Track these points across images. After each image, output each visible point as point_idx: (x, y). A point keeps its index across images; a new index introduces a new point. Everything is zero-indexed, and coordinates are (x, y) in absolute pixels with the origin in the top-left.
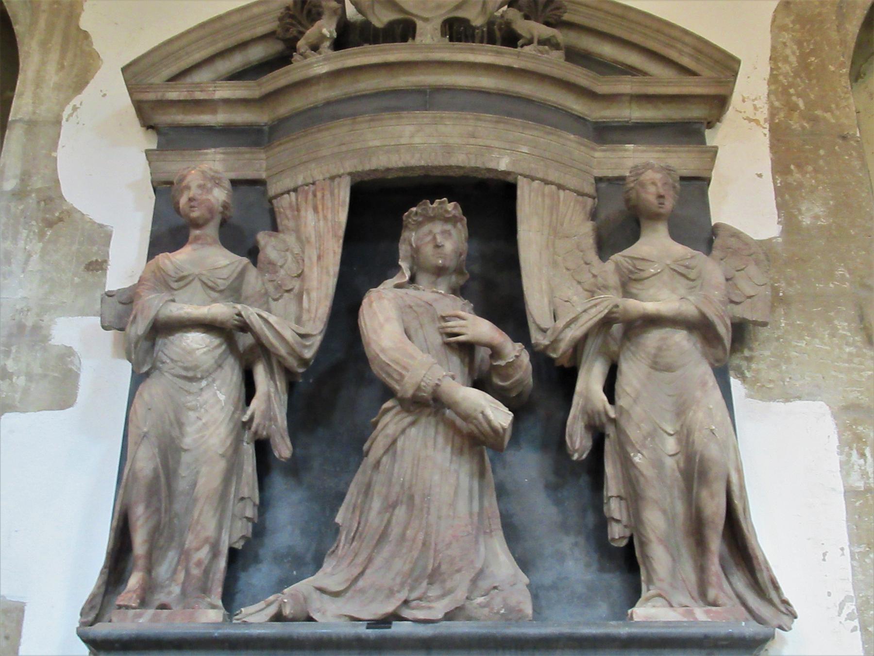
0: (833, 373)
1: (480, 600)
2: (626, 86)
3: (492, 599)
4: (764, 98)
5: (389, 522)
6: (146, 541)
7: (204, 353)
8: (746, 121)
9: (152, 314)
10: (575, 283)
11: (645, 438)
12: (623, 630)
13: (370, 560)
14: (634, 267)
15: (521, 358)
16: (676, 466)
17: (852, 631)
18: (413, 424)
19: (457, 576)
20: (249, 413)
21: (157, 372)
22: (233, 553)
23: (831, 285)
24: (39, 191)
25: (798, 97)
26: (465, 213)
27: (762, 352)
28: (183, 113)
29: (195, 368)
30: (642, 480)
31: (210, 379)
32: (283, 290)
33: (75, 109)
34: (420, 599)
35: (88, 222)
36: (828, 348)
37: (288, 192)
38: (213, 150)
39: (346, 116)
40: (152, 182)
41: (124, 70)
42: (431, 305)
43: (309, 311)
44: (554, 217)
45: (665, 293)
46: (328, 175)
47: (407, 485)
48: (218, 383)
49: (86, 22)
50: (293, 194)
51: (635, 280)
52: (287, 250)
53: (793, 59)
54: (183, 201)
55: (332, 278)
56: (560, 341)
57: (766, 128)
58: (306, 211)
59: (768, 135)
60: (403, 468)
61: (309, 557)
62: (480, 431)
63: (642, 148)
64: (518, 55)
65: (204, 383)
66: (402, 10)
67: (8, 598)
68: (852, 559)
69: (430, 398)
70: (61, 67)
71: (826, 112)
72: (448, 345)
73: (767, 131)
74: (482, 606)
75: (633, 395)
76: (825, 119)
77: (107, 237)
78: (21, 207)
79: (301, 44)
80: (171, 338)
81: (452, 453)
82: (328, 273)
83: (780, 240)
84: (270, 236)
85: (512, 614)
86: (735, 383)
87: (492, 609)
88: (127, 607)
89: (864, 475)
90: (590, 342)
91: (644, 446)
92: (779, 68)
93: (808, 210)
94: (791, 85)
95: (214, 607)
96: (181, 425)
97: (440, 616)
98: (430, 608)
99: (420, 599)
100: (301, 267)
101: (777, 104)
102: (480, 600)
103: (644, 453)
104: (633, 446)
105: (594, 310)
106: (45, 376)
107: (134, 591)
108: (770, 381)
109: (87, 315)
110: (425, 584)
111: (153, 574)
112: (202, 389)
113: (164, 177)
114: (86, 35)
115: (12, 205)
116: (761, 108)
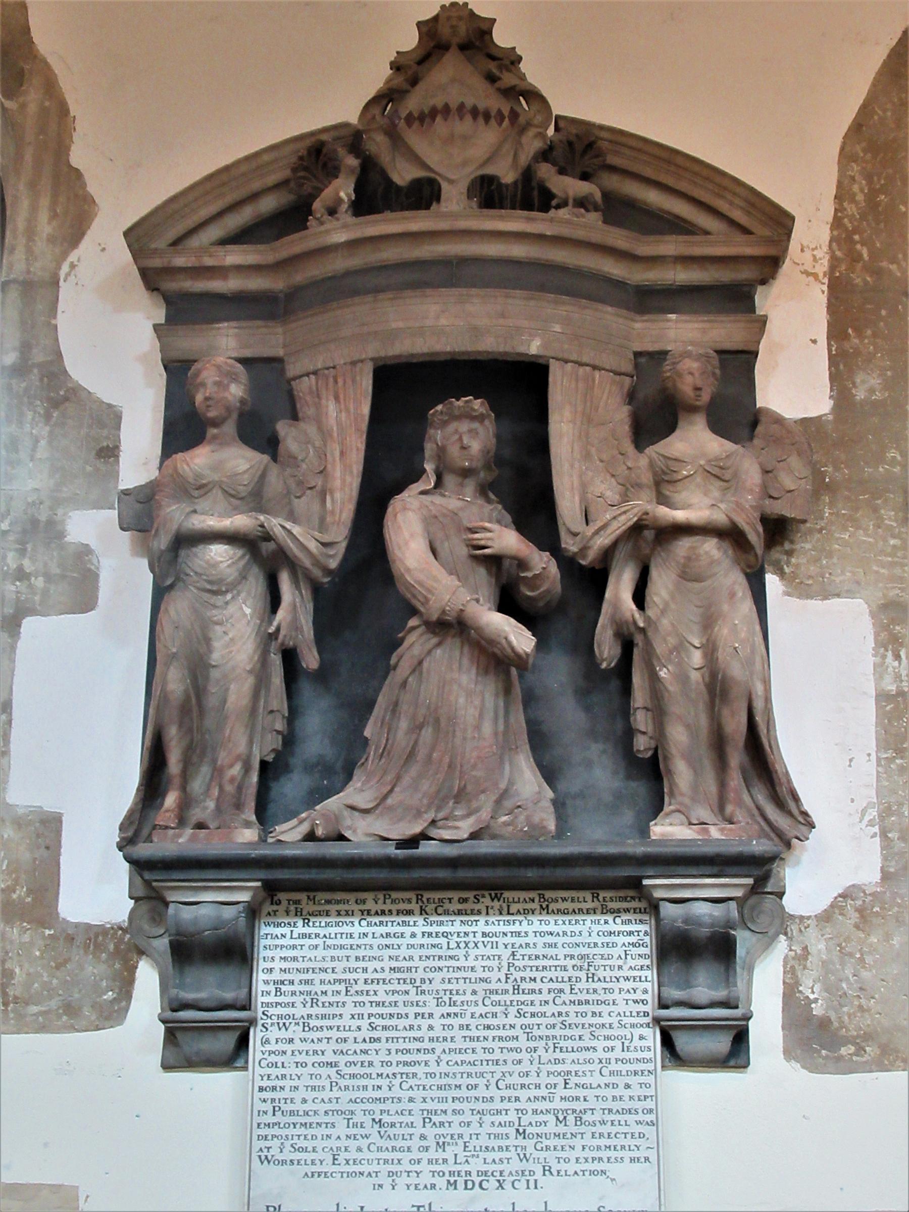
0: (875, 568)
1: (505, 818)
2: (670, 246)
3: (516, 817)
4: (825, 248)
5: (416, 742)
6: (179, 761)
7: (229, 566)
8: (804, 275)
9: (175, 527)
10: (608, 477)
11: (671, 653)
12: (640, 849)
13: (398, 778)
14: (667, 467)
15: (548, 569)
16: (701, 680)
17: (872, 837)
18: (439, 645)
19: (482, 797)
20: (275, 623)
21: (181, 584)
22: (264, 764)
23: (881, 469)
24: (40, 365)
25: (862, 245)
26: (492, 408)
27: (803, 545)
28: (192, 278)
29: (220, 581)
30: (666, 694)
31: (235, 592)
32: (304, 487)
33: (73, 266)
34: (446, 819)
35: (95, 402)
36: (871, 540)
37: (308, 375)
38: (226, 324)
39: (367, 292)
40: (162, 360)
41: (127, 234)
42: (456, 514)
43: (333, 512)
44: (588, 404)
46: (349, 360)
47: (433, 706)
48: (243, 595)
49: (78, 157)
50: (313, 377)
51: (668, 482)
52: (308, 442)
53: (860, 197)
54: (199, 398)
55: (355, 479)
56: (589, 548)
57: (824, 284)
58: (327, 400)
59: (826, 292)
60: (429, 691)
61: (339, 765)
62: (505, 656)
63: (684, 317)
64: (552, 220)
65: (229, 596)
66: (425, 166)
67: (45, 809)
68: (878, 765)
69: (454, 622)
70: (54, 216)
71: (892, 263)
72: (475, 558)
73: (825, 288)
74: (506, 824)
75: (661, 607)
76: (890, 271)
77: (117, 418)
78: (23, 385)
79: (317, 205)
80: (194, 550)
81: (478, 674)
82: (351, 472)
83: (830, 417)
84: (291, 426)
85: (535, 832)
86: (772, 581)
87: (517, 827)
88: (167, 827)
89: (898, 677)
90: (620, 546)
91: (670, 660)
92: (845, 209)
93: (863, 382)
94: (855, 231)
95: (247, 824)
96: (208, 641)
97: (466, 836)
98: (457, 828)
99: (446, 819)
100: (323, 463)
101: (838, 253)
102: (505, 818)
103: (670, 667)
104: (659, 659)
105: (623, 518)
106: (63, 577)
107: (173, 811)
108: (810, 577)
109: (102, 508)
110: (451, 804)
111: (188, 789)
112: (227, 603)
113: (175, 354)
114: (78, 173)
115: (14, 382)
116: (821, 259)
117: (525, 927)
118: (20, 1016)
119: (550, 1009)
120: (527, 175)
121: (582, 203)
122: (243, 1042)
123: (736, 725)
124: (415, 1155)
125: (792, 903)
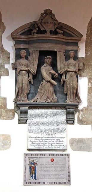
12: (65, 103)
22: (28, 93)
45: (72, 68)
117: (54, 111)
118: (3, 118)
119: (56, 119)
120: (56, 30)
121: (61, 33)
122: (27, 121)
123: (75, 92)
124: (43, 132)
125: (79, 108)
